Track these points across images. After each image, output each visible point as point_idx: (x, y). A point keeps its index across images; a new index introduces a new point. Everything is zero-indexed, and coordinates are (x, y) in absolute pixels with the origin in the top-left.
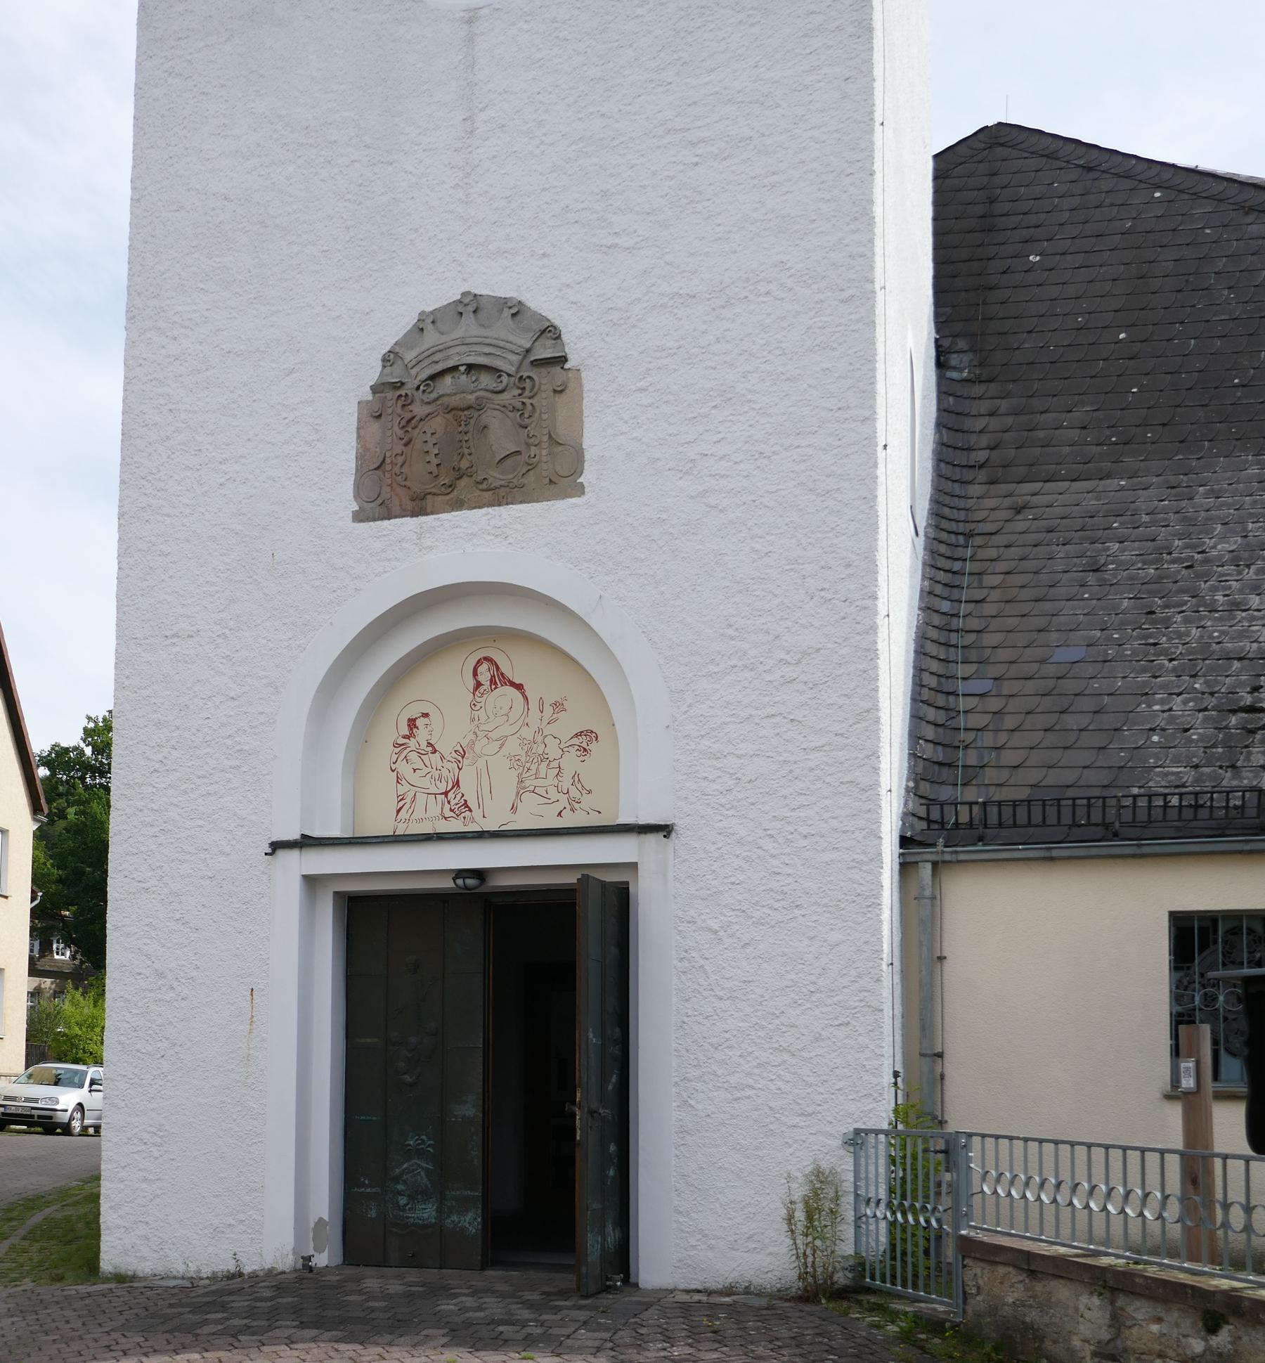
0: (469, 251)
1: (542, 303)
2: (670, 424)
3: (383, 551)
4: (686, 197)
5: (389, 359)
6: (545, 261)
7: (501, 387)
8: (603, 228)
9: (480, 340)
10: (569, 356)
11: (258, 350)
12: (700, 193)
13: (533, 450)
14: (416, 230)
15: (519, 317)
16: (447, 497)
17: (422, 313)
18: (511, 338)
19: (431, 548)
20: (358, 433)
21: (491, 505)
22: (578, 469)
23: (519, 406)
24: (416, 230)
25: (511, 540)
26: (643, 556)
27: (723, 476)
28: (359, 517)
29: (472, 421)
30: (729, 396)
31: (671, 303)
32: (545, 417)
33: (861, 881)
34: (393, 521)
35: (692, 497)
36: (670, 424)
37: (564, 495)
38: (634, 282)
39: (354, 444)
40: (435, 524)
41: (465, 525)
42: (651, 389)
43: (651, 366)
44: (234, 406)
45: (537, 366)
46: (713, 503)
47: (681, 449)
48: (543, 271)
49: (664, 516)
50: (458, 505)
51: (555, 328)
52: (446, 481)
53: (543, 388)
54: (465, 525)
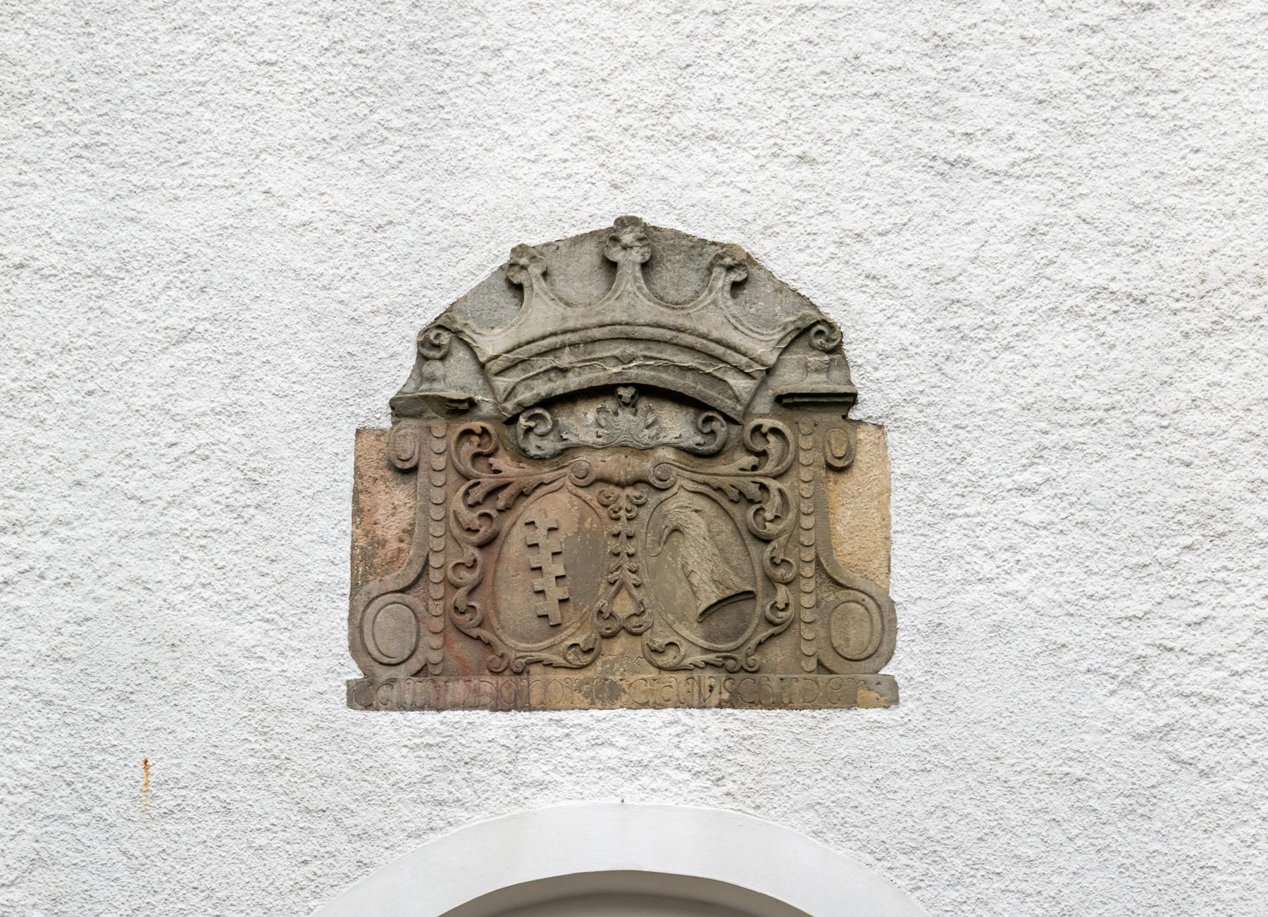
0: (623, 121)
1: (802, 264)
2: (1089, 572)
3: (426, 781)
4: (1125, 78)
5: (439, 340)
6: (805, 172)
7: (713, 447)
8: (935, 118)
9: (669, 334)
10: (862, 395)
11: (97, 272)
12: (1157, 73)
13: (782, 594)
14: (498, 52)
15: (746, 292)
16: (580, 675)
17: (520, 250)
18: (736, 338)
19: (541, 785)
20: (356, 501)
21: (680, 704)
22: (882, 647)
23: (753, 490)
24: (498, 52)
25: (730, 786)
26: (1031, 853)
27: (1206, 700)
28: (362, 696)
29: (644, 513)
30: (1221, 528)
31: (1091, 308)
32: (807, 522)
33: (908, 577)
34: (449, 715)
35: (1139, 737)
36: (1089, 572)
37: (849, 701)
38: (1011, 248)
39: (347, 525)
40: (550, 731)
41: (622, 742)
42: (1047, 491)
43: (1046, 441)
44: (35, 397)
45: (787, 406)
46: (1186, 755)
47: (1114, 630)
48: (803, 195)
49: (1078, 771)
50: (606, 695)
51: (831, 327)
52: (579, 639)
53: (804, 457)
54: (622, 742)
